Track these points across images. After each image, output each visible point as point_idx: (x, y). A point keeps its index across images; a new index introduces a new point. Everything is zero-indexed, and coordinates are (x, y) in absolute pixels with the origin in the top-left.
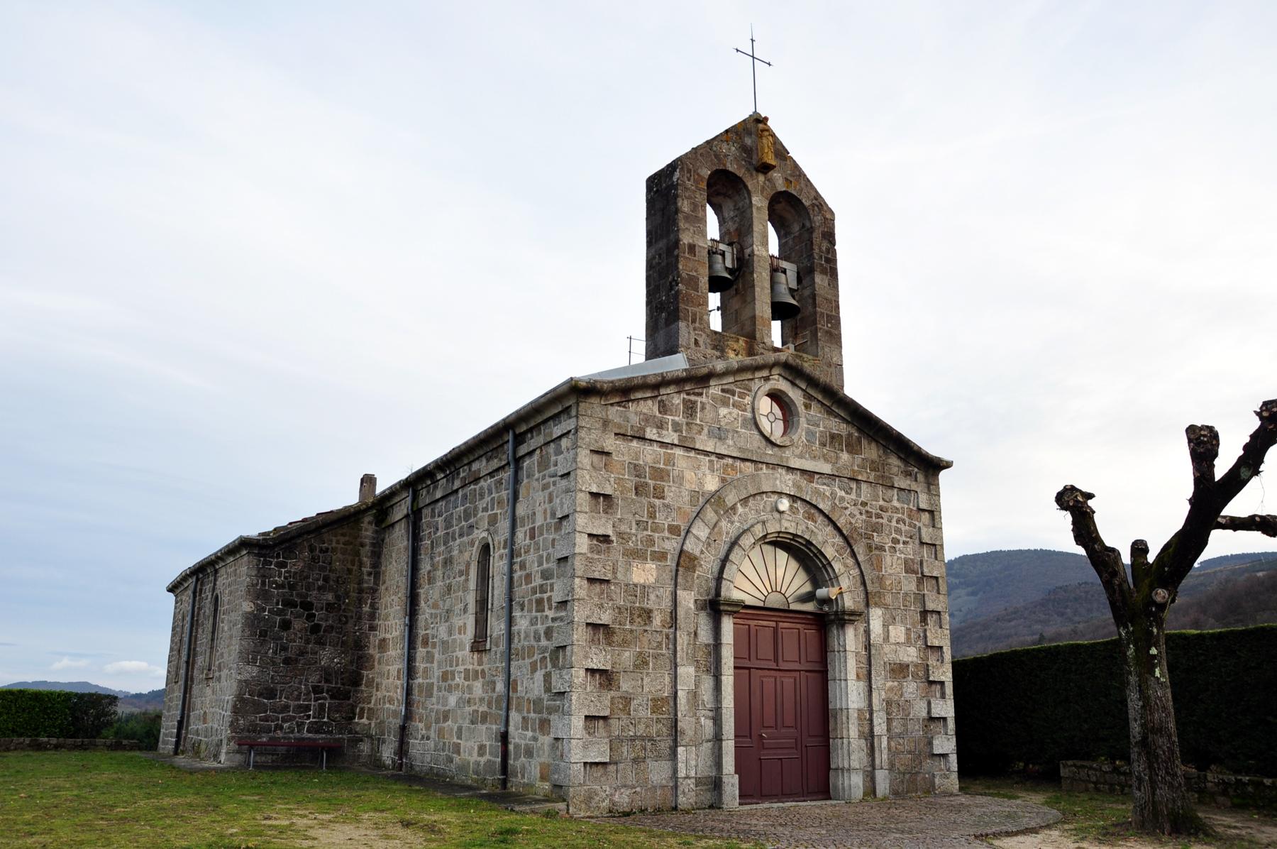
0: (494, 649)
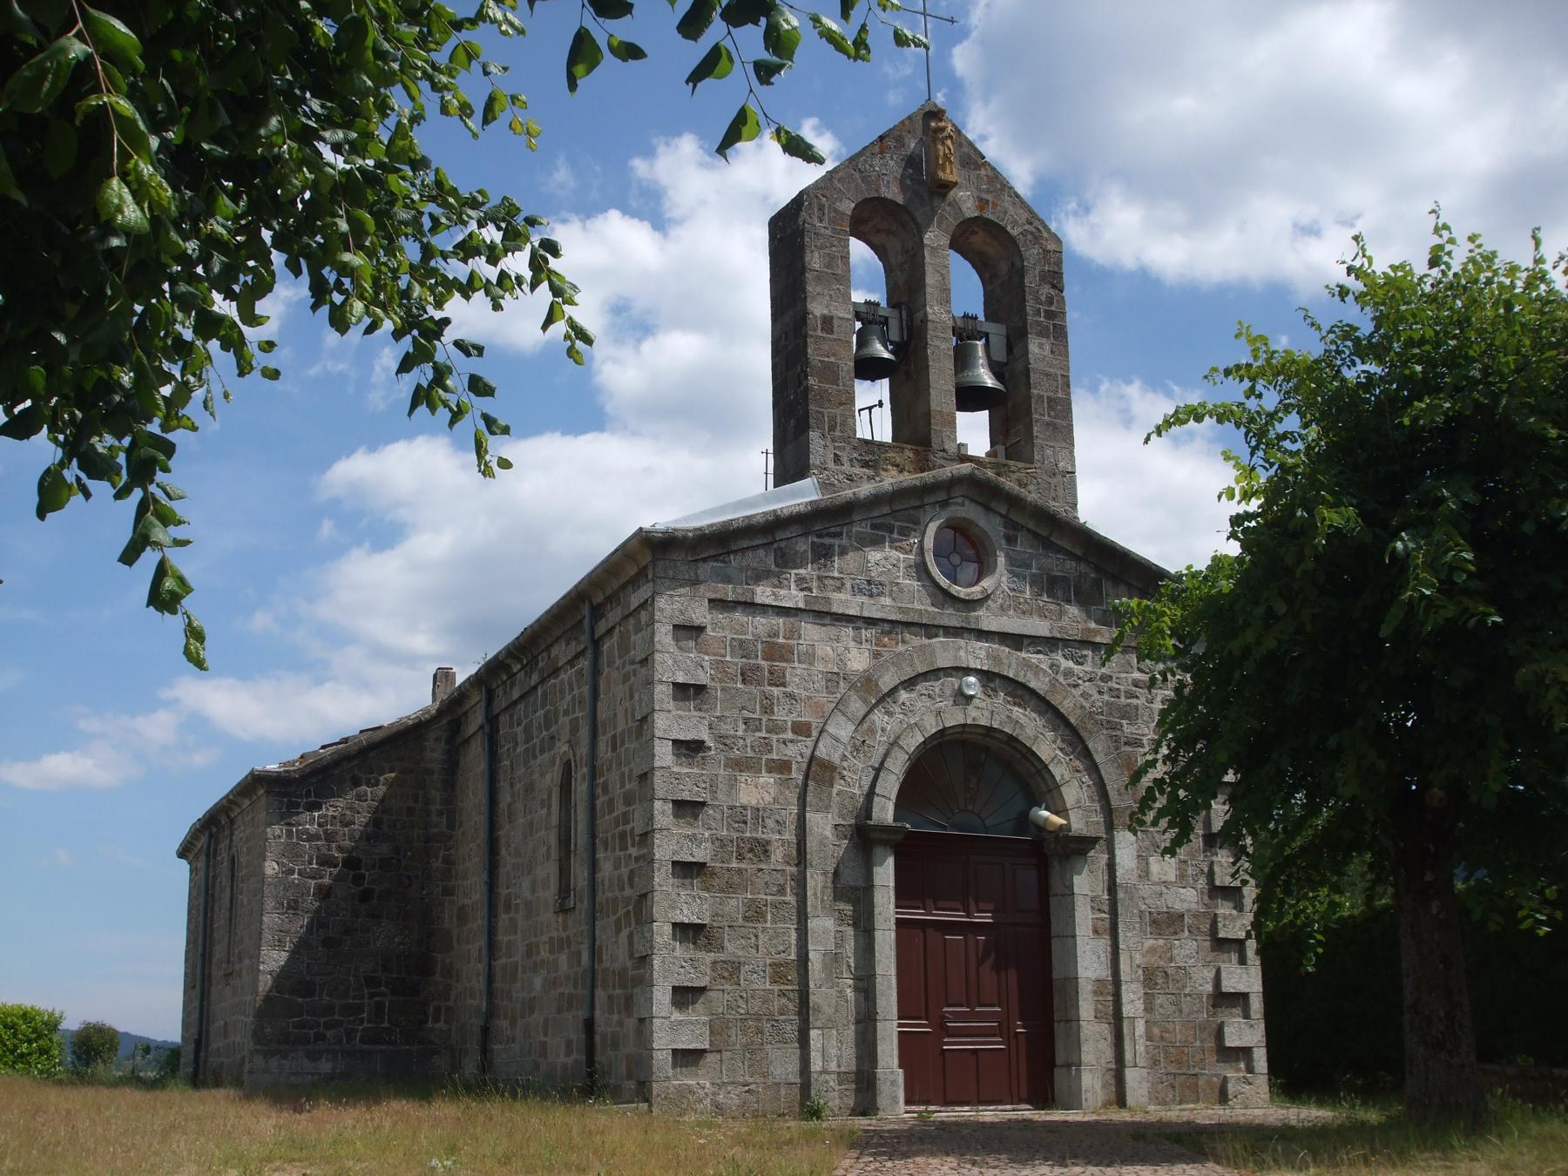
0: (578, 905)
